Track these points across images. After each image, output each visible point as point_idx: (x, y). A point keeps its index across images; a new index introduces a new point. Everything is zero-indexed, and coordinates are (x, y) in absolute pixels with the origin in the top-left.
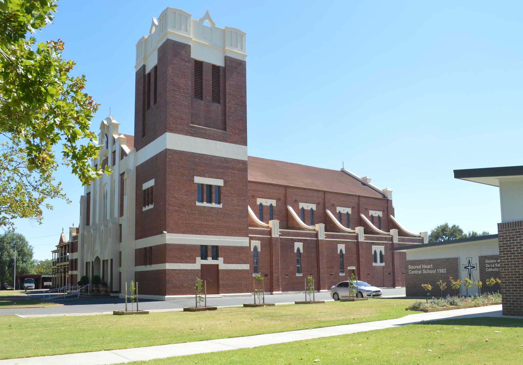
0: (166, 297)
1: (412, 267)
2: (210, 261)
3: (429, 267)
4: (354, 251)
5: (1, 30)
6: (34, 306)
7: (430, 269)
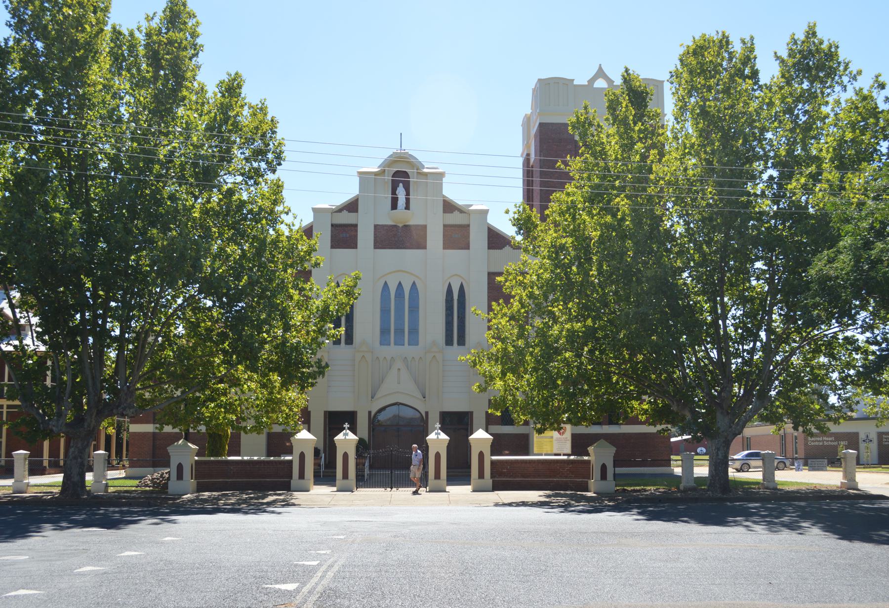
3: (830, 439)
5: (888, 195)
6: (116, 475)
7: (831, 441)
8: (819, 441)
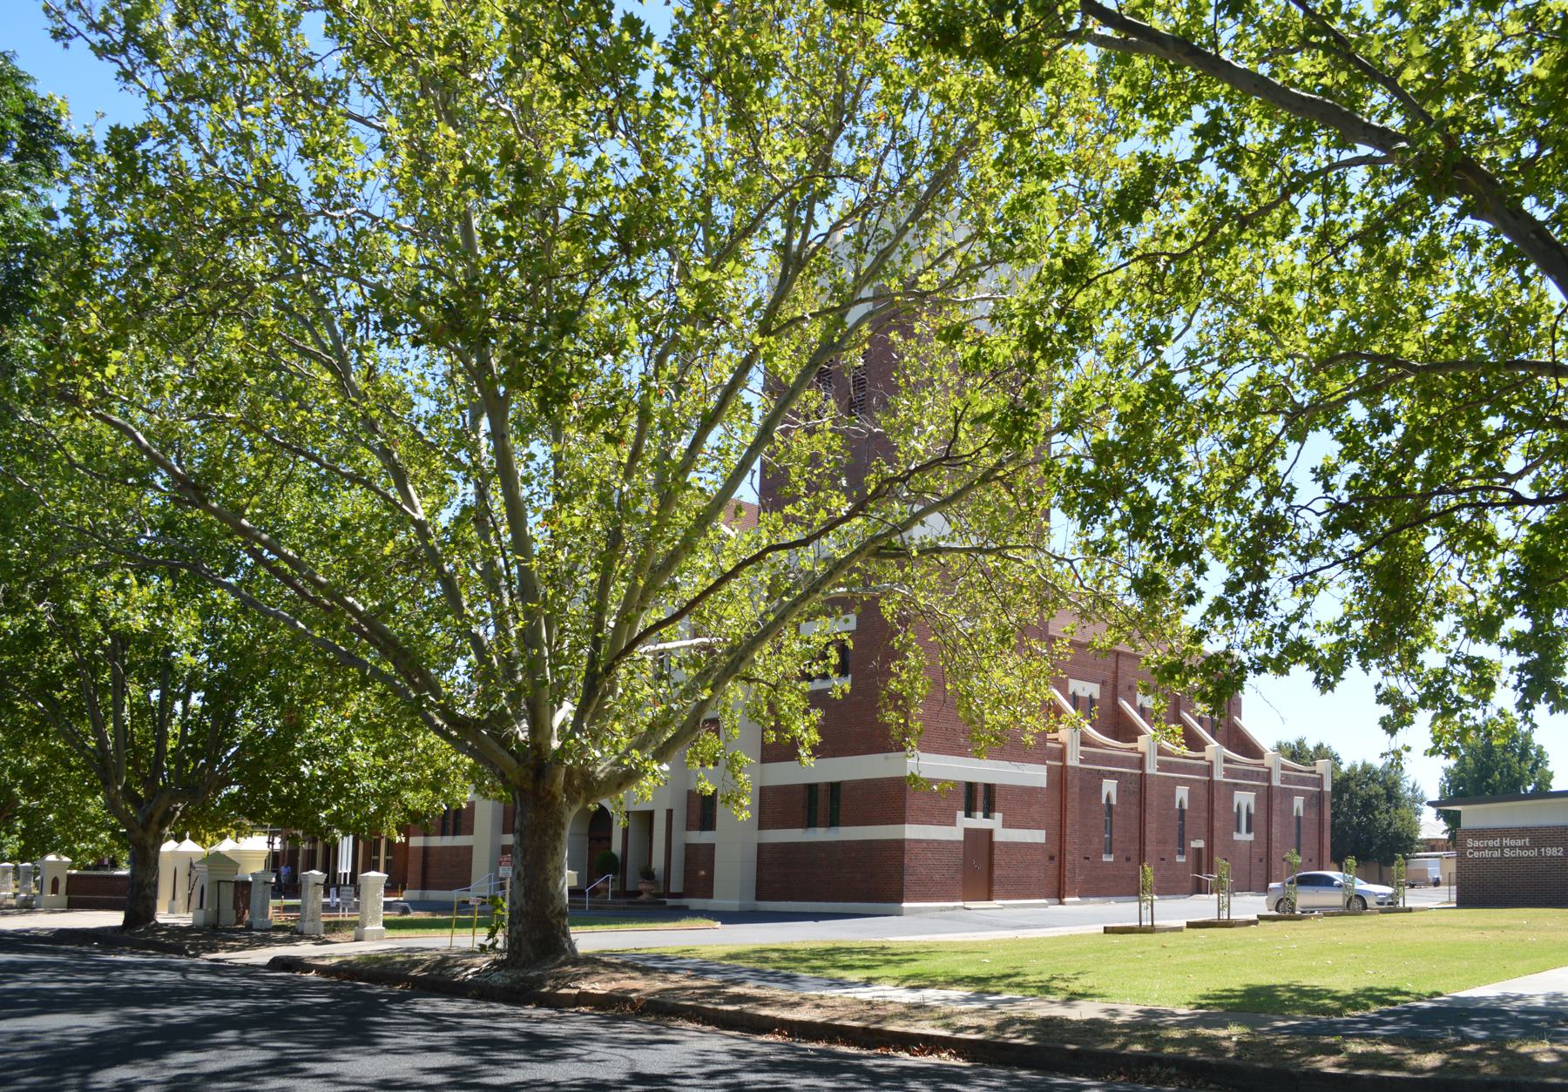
0: (905, 905)
1: (1477, 844)
2: (979, 822)
3: (1520, 843)
4: (1204, 804)
7: (1521, 848)
8: (1495, 848)
